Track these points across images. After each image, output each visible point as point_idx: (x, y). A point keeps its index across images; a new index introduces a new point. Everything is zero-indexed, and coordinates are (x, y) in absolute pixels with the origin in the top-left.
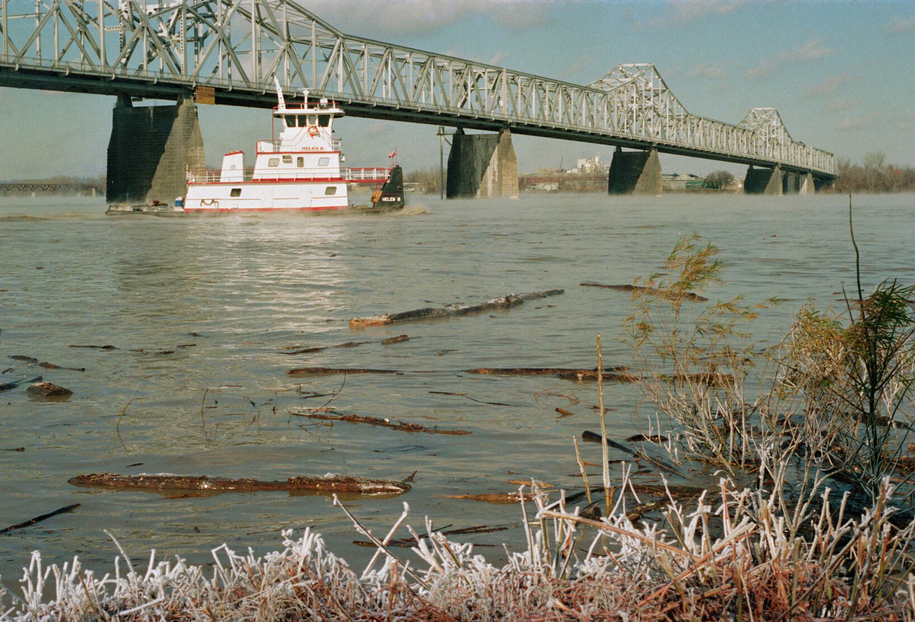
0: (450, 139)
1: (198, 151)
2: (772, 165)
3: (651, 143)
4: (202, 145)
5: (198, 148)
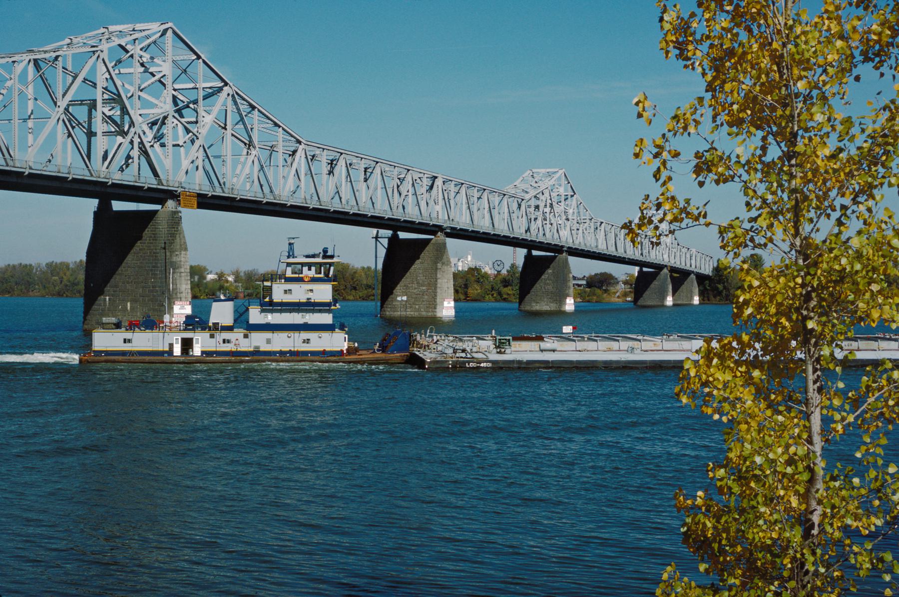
0: (385, 242)
1: (182, 255)
2: (659, 267)
3: (562, 247)
4: (186, 249)
5: (183, 252)
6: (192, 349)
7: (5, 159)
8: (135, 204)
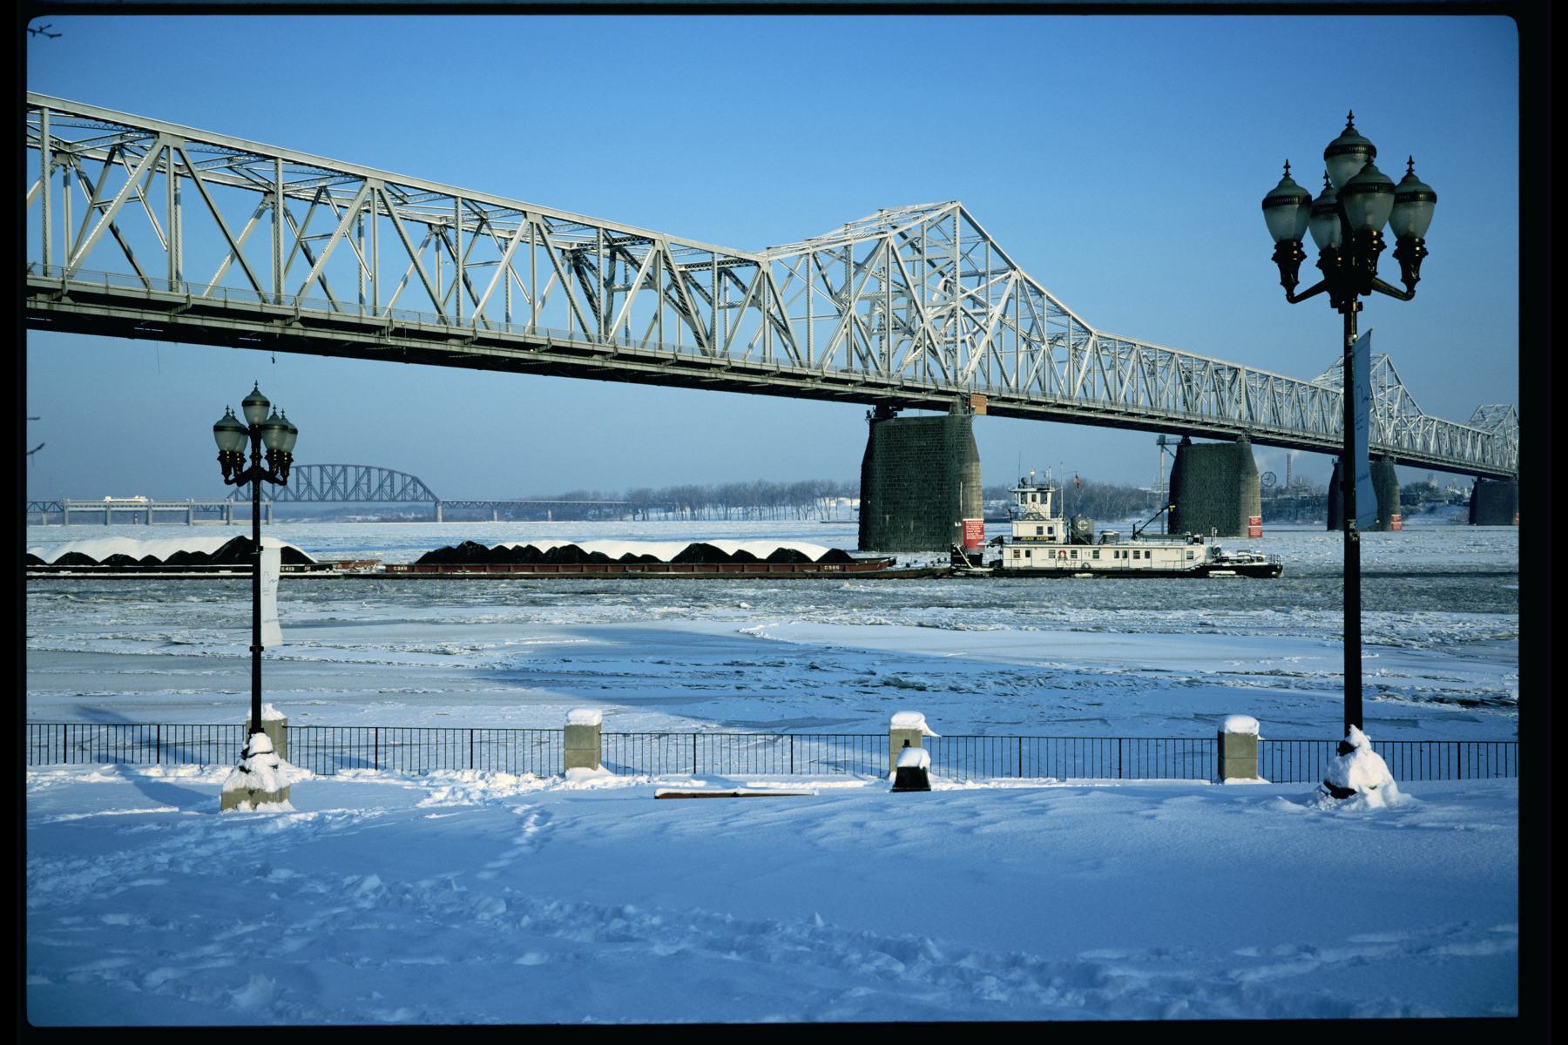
0: (1174, 449)
6: (295, 522)
7: (600, 332)
8: (917, 410)
